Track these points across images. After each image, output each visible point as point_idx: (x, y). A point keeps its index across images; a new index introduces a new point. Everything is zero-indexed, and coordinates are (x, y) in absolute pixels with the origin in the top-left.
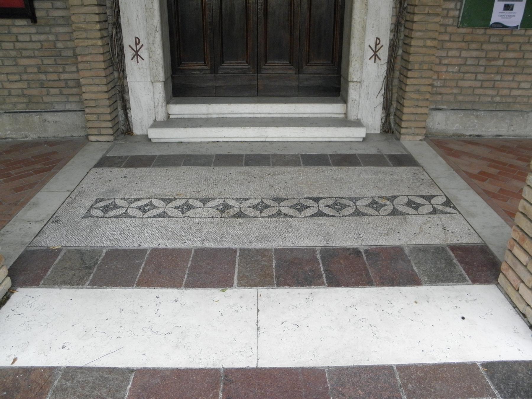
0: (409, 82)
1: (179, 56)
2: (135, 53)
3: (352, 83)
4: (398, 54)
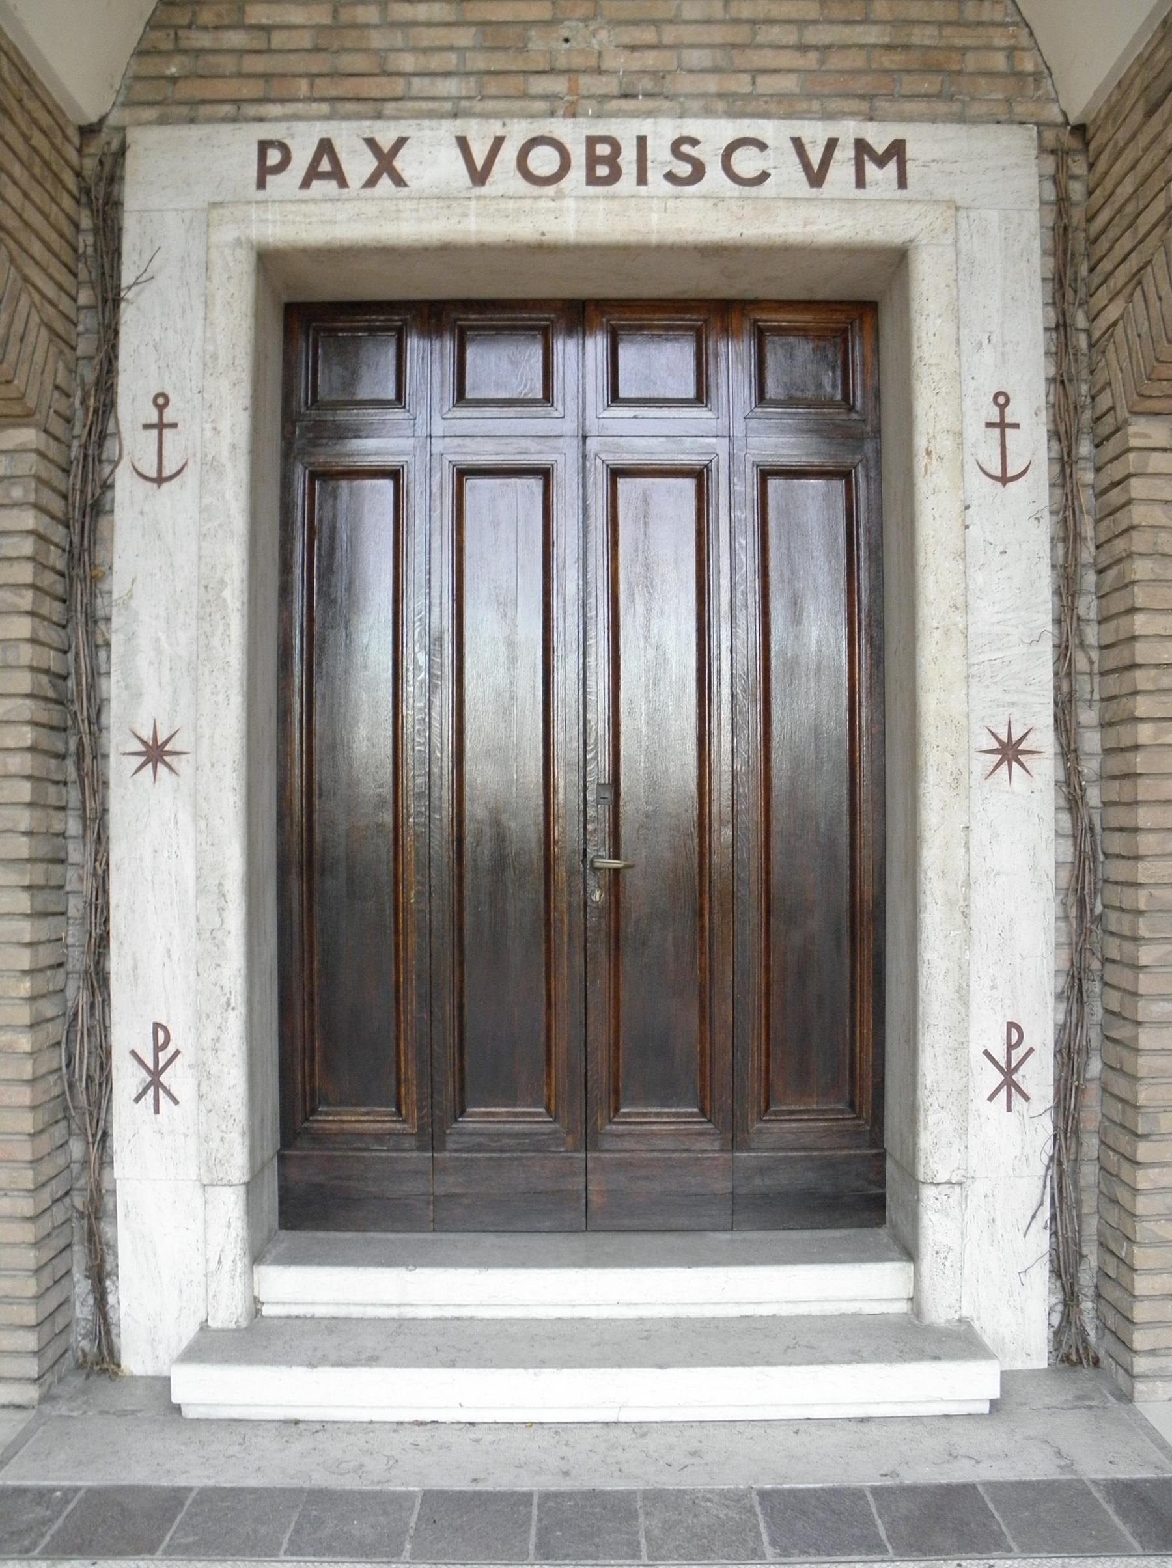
0: (1144, 1179)
1: (308, 1087)
2: (149, 1079)
3: (933, 1188)
4: (1088, 1076)
